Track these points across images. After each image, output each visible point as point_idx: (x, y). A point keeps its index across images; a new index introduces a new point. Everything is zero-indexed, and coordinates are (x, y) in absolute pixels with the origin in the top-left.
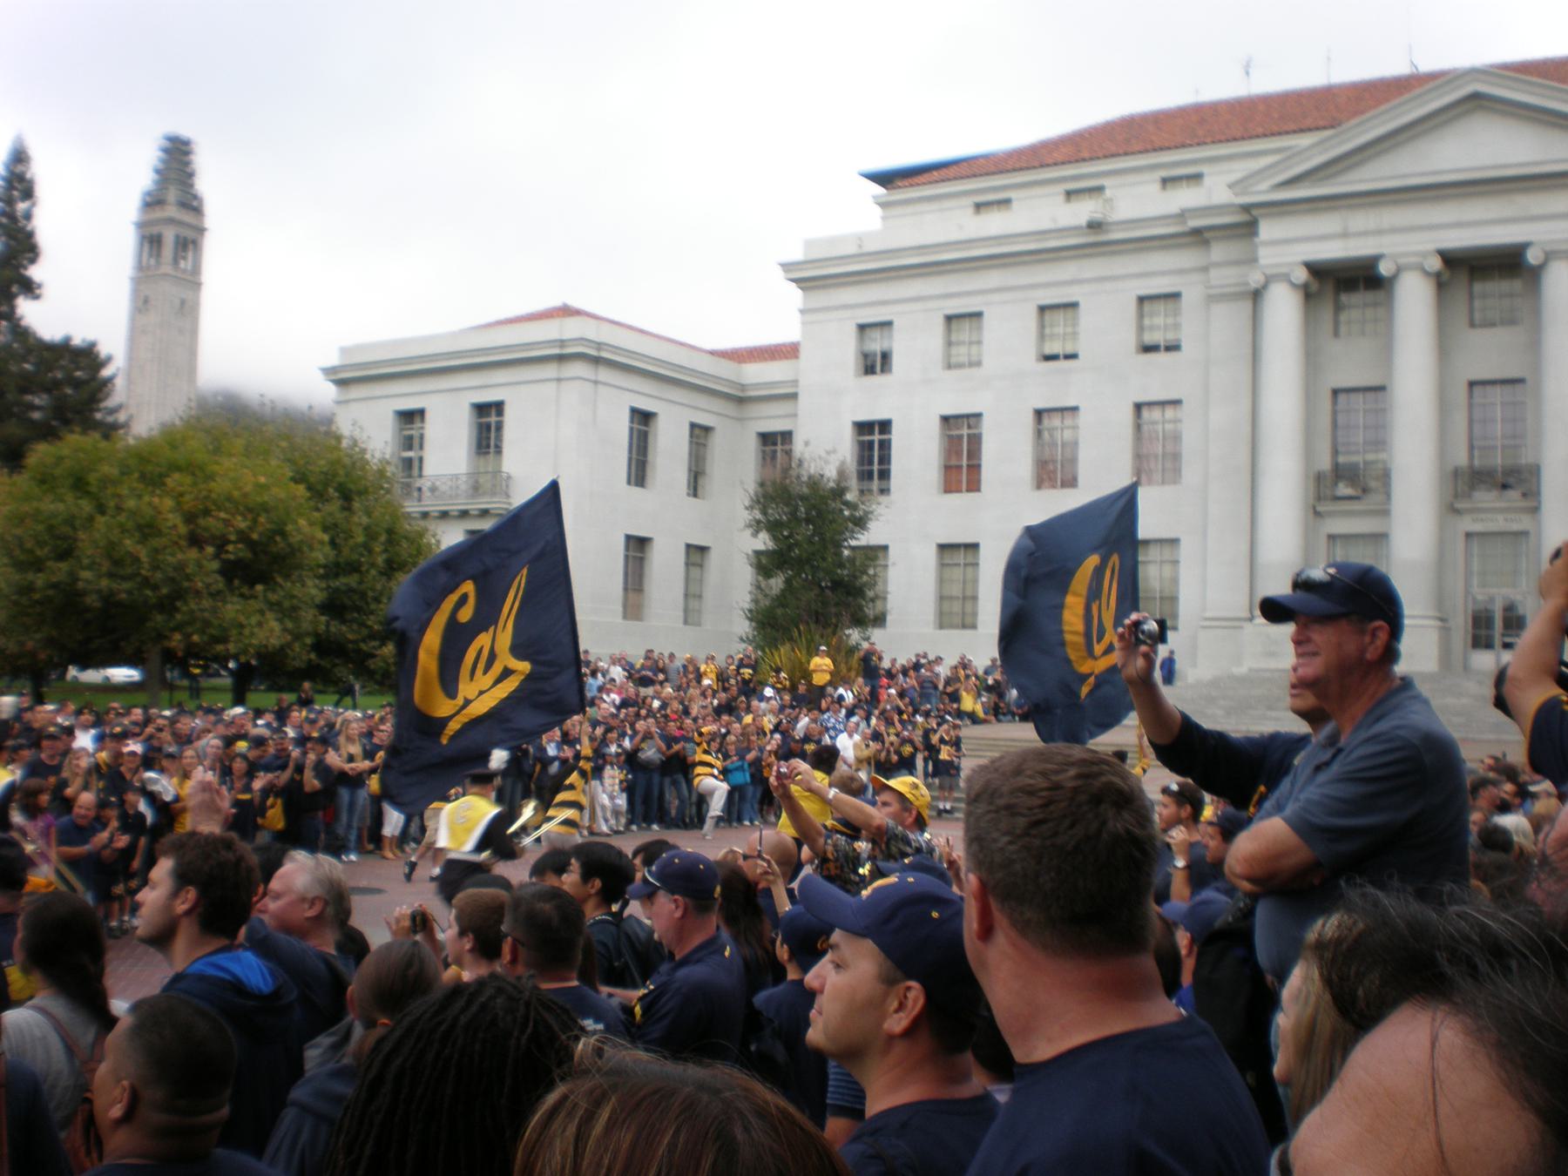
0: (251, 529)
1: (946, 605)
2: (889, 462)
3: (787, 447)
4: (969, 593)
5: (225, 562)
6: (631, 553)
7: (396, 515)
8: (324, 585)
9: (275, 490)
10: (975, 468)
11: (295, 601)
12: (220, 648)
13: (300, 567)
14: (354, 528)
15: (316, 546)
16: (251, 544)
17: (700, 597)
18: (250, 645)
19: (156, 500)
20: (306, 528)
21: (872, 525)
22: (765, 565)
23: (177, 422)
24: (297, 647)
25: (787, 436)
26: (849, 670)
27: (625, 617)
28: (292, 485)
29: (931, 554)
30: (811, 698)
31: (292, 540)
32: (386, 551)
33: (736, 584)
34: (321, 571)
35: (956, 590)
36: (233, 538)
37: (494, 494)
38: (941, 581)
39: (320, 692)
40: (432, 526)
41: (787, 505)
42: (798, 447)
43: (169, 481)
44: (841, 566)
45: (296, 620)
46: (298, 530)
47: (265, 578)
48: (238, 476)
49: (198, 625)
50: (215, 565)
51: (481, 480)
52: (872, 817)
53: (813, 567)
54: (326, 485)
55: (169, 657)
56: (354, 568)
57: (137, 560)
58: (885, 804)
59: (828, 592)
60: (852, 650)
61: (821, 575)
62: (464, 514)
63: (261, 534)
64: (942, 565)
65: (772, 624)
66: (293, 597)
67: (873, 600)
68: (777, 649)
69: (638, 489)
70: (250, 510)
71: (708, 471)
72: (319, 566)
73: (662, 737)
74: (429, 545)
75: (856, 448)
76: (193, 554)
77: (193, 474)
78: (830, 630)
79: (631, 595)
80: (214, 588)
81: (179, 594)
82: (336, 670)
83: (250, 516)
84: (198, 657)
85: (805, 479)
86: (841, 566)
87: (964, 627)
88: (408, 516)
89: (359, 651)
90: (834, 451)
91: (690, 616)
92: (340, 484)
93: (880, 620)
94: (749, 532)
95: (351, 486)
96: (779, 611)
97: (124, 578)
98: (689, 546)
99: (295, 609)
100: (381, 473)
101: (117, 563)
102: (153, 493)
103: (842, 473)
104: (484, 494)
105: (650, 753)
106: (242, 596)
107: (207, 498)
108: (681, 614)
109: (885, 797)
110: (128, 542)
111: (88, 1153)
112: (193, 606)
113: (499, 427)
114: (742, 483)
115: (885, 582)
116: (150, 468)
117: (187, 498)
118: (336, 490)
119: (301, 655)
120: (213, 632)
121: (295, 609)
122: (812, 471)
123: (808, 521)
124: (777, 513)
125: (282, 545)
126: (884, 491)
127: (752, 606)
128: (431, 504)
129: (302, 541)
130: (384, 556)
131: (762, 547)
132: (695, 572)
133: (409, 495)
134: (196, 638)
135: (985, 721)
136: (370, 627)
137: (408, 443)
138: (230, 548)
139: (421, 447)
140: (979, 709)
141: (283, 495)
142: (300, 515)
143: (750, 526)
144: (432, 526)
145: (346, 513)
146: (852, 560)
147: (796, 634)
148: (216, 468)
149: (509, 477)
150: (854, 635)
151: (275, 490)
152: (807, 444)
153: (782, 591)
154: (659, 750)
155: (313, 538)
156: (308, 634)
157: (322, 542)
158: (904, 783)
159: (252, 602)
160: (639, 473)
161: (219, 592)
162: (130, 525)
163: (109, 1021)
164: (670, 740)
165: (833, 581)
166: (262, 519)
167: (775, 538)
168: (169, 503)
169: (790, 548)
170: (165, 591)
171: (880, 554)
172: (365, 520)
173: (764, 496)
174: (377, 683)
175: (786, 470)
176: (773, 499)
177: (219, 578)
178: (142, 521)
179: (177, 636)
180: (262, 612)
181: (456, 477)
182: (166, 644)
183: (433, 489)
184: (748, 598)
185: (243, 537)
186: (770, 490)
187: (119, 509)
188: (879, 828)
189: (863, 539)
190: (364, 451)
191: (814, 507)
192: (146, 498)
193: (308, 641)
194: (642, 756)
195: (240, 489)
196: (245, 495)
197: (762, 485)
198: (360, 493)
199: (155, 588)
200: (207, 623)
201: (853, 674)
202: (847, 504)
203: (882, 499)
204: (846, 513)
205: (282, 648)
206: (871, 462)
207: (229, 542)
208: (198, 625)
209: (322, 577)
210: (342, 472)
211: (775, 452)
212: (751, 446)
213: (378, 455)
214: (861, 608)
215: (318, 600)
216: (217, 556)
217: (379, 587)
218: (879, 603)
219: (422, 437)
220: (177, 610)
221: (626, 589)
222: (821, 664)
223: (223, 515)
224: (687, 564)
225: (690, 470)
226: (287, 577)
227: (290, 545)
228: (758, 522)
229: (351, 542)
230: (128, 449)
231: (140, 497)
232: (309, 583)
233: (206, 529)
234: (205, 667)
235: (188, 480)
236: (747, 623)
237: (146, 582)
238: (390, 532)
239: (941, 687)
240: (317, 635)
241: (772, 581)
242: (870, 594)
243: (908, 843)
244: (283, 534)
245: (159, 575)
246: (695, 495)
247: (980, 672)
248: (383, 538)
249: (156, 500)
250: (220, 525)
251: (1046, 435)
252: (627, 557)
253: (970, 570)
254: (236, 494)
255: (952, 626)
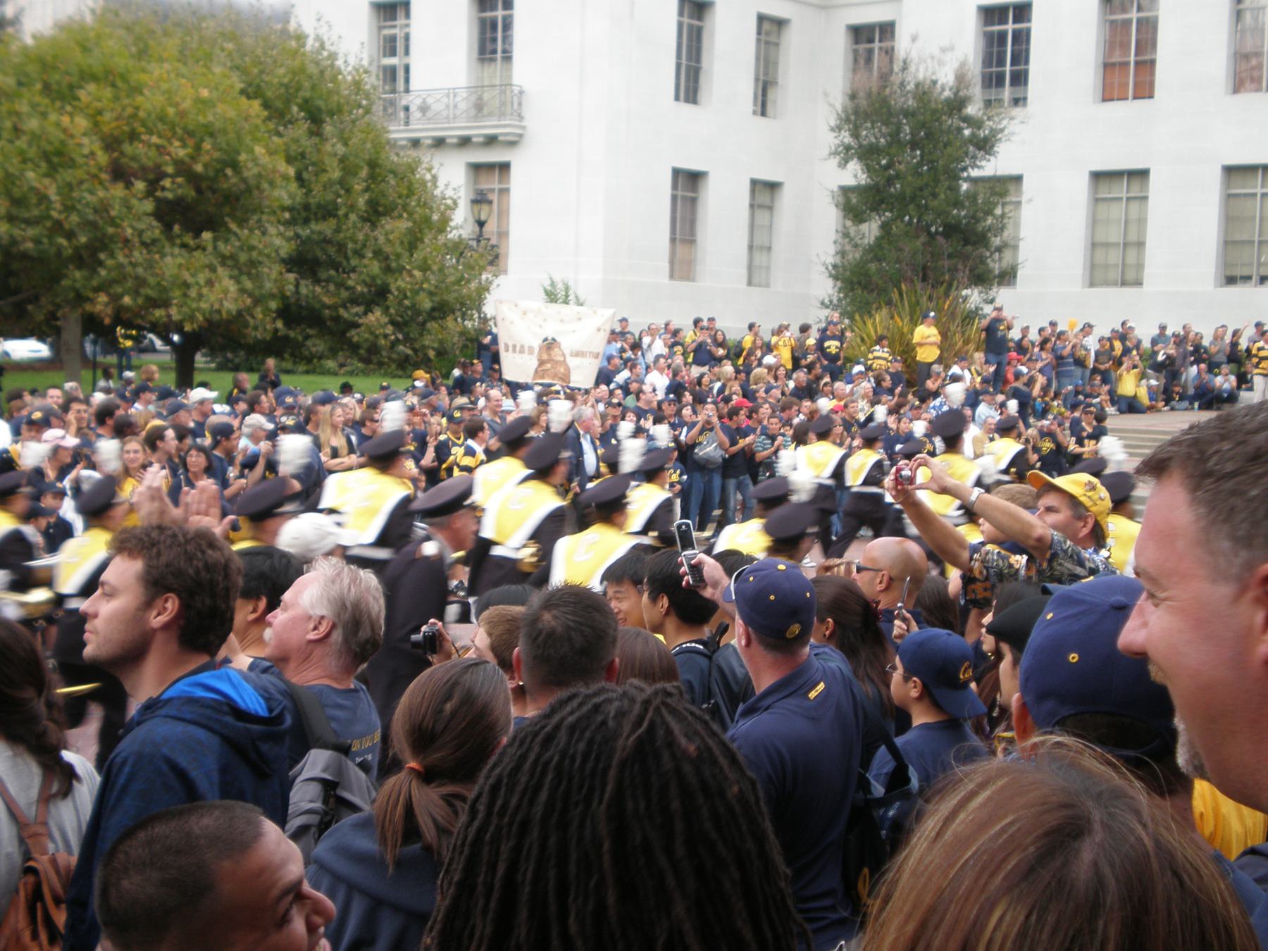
0: (193, 158)
1: (1100, 253)
2: (1027, 62)
3: (886, 44)
4: (1133, 237)
5: (159, 201)
6: (680, 193)
7: (381, 144)
8: (290, 234)
9: (220, 108)
10: (1146, 67)
11: (254, 254)
12: (159, 313)
13: (258, 209)
14: (327, 160)
15: (279, 181)
16: (193, 178)
17: (769, 249)
18: (198, 309)
19: (66, 120)
20: (265, 158)
21: (1001, 148)
22: (855, 205)
23: (89, 19)
24: (258, 313)
25: (887, 30)
26: (966, 342)
27: (672, 276)
28: (244, 100)
29: (1082, 184)
30: (913, 381)
31: (246, 174)
32: (367, 189)
33: (815, 234)
34: (287, 215)
35: (1115, 235)
36: (170, 170)
37: (502, 115)
38: (1094, 222)
39: (288, 372)
40: (426, 157)
41: (886, 123)
42: (902, 44)
43: (82, 94)
44: (957, 204)
45: (256, 278)
46: (255, 160)
47: (212, 223)
48: (170, 88)
49: (130, 283)
50: (149, 206)
51: (486, 97)
52: (1031, 526)
53: (919, 206)
54: (288, 102)
55: (92, 324)
56: (327, 212)
57: (43, 198)
58: (1049, 510)
59: (940, 239)
60: (971, 316)
61: (929, 217)
62: (465, 142)
63: (206, 166)
64: (1096, 201)
65: (862, 284)
66: (252, 248)
67: (999, 250)
68: (871, 316)
69: (688, 108)
70: (191, 134)
71: (780, 81)
72: (284, 209)
73: (725, 429)
74: (424, 183)
75: (981, 44)
76: (118, 191)
77: (113, 85)
78: (942, 290)
79: (680, 248)
80: (147, 237)
81: (101, 244)
82: (309, 343)
83: (191, 142)
84: (128, 325)
85: (911, 87)
86: (957, 204)
87: (1124, 284)
88: (393, 144)
89: (337, 319)
90: (952, 48)
91: (755, 275)
92: (306, 101)
93: (1008, 277)
94: (835, 161)
95: (321, 103)
96: (873, 267)
97: (28, 222)
98: (754, 183)
99: (253, 263)
100: (357, 84)
101: (18, 202)
102: (61, 111)
103: (961, 78)
104: (490, 114)
105: (710, 449)
106: (184, 246)
107: (134, 116)
108: (744, 272)
109: (1050, 500)
110: (31, 175)
111: (35, 936)
112: (121, 258)
113: (508, 25)
114: (826, 95)
115: (1017, 225)
116: (57, 77)
117: (108, 116)
118: (301, 108)
119: (264, 324)
120: (150, 292)
121: (253, 263)
122: (921, 76)
123: (914, 145)
124: (872, 134)
125: (234, 180)
126: (1018, 101)
127: (838, 260)
128: (422, 129)
129: (260, 175)
130: (367, 196)
131: (851, 182)
132: (762, 216)
133: (391, 116)
134: (127, 300)
135: (1151, 409)
136: (353, 288)
137: (390, 46)
138: (167, 183)
139: (407, 52)
140: (1143, 395)
141: (231, 114)
142: (256, 140)
143: (836, 153)
144: (426, 157)
145: (316, 140)
146: (972, 197)
147: (895, 296)
148: (143, 77)
149: (521, 92)
150: (973, 296)
151: (220, 108)
152: (914, 39)
153: (877, 239)
154: (721, 445)
155: (274, 171)
156: (273, 296)
157: (286, 178)
158: (1075, 482)
159: (197, 254)
160: (689, 84)
161: (154, 241)
162: (32, 152)
163: (69, 774)
164: (736, 434)
165: (946, 226)
166: (207, 145)
167: (869, 169)
168: (82, 123)
169: (890, 181)
170: (83, 239)
171: (1012, 187)
172: (341, 149)
173: (856, 113)
174: (362, 360)
175: (885, 77)
176: (867, 116)
177: (155, 223)
178: (49, 148)
179: (103, 298)
180: (213, 269)
181: (451, 92)
182: (88, 307)
183: (424, 109)
184: (832, 249)
185: (183, 169)
186: (863, 103)
187: (17, 130)
188: (1040, 539)
189: (989, 167)
190: (333, 56)
191: (923, 125)
192: (53, 117)
193: (273, 305)
194: (700, 452)
195: (176, 105)
196: (183, 114)
197: (853, 97)
198: (331, 113)
199: (70, 235)
200: (141, 282)
201: (972, 347)
202: (968, 120)
203: (1017, 112)
204: (967, 132)
205: (240, 314)
206: (1001, 62)
207: (164, 175)
208: (130, 283)
209: (287, 223)
210: (307, 84)
211: (870, 51)
212: (839, 43)
213: (352, 61)
214: (982, 261)
215: (283, 253)
216: (150, 193)
217: (361, 237)
218: (1007, 256)
219: (407, 38)
220: (101, 263)
221: (673, 240)
222: (926, 334)
223: (155, 139)
224: (752, 206)
225: (757, 80)
226: (242, 223)
227: (244, 180)
228: (848, 148)
229: (324, 178)
230: (25, 50)
231: (44, 115)
232: (272, 230)
233: (134, 158)
234: (138, 340)
235: (108, 93)
236: (830, 282)
237: (58, 227)
238: (373, 165)
239: (1091, 363)
240: (284, 297)
241: (864, 227)
242: (996, 241)
243: (1081, 563)
244: (235, 165)
245: (74, 218)
246: (763, 113)
247: (1146, 344)
248: (364, 173)
249: (66, 120)
250: (153, 153)
251: (1248, 18)
252: (674, 198)
253: (1134, 206)
254: (171, 111)
255: (1107, 283)
